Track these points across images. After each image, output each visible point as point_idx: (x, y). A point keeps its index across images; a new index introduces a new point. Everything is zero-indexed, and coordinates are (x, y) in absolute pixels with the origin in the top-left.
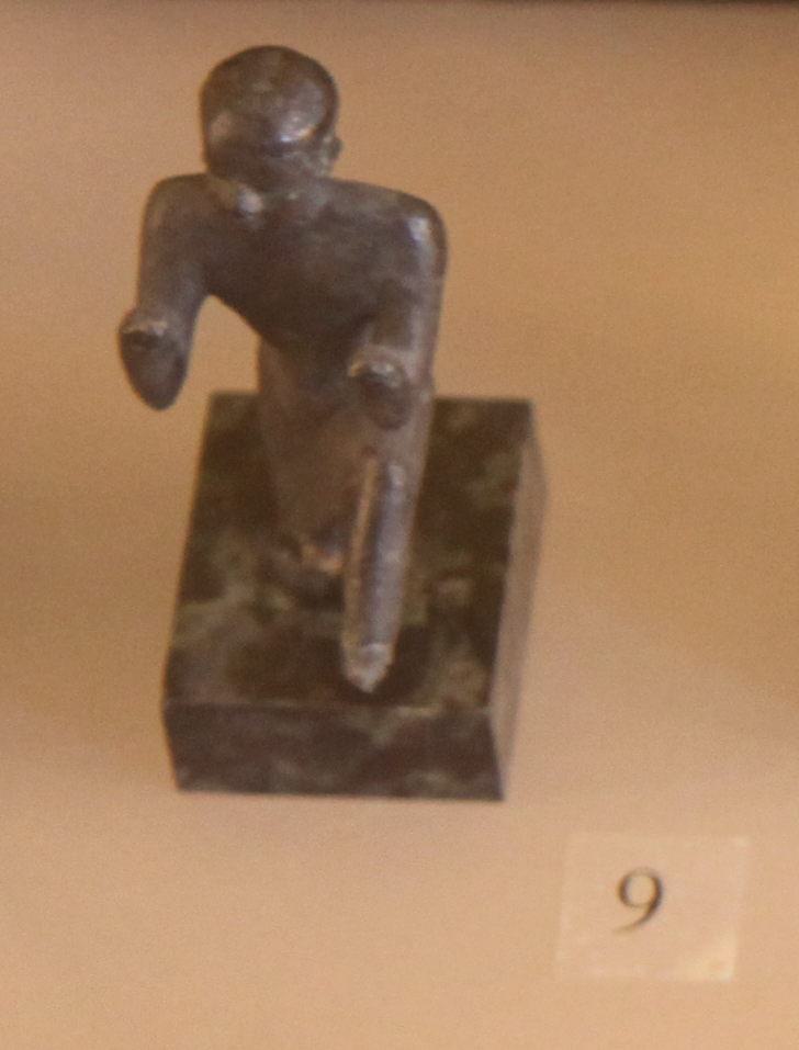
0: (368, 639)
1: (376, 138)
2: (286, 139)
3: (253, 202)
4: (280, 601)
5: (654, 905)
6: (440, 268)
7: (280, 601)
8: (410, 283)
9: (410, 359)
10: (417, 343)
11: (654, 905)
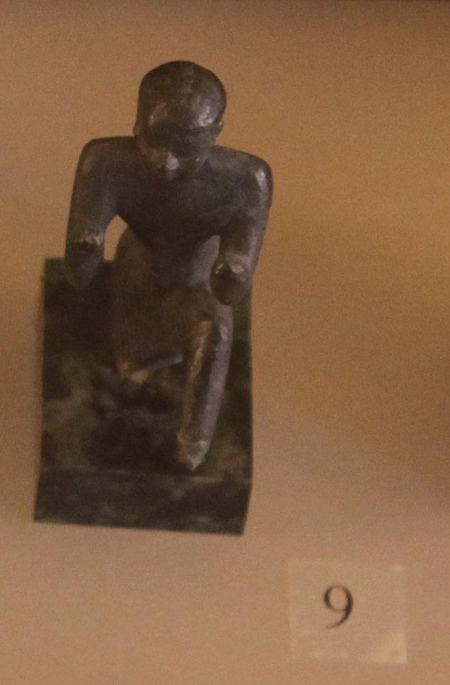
0: (196, 438)
1: (241, 125)
2: (202, 124)
3: (173, 163)
4: (108, 402)
5: (348, 609)
6: (269, 205)
7: (108, 402)
8: (252, 213)
9: (248, 260)
10: (252, 252)
11: (327, 598)
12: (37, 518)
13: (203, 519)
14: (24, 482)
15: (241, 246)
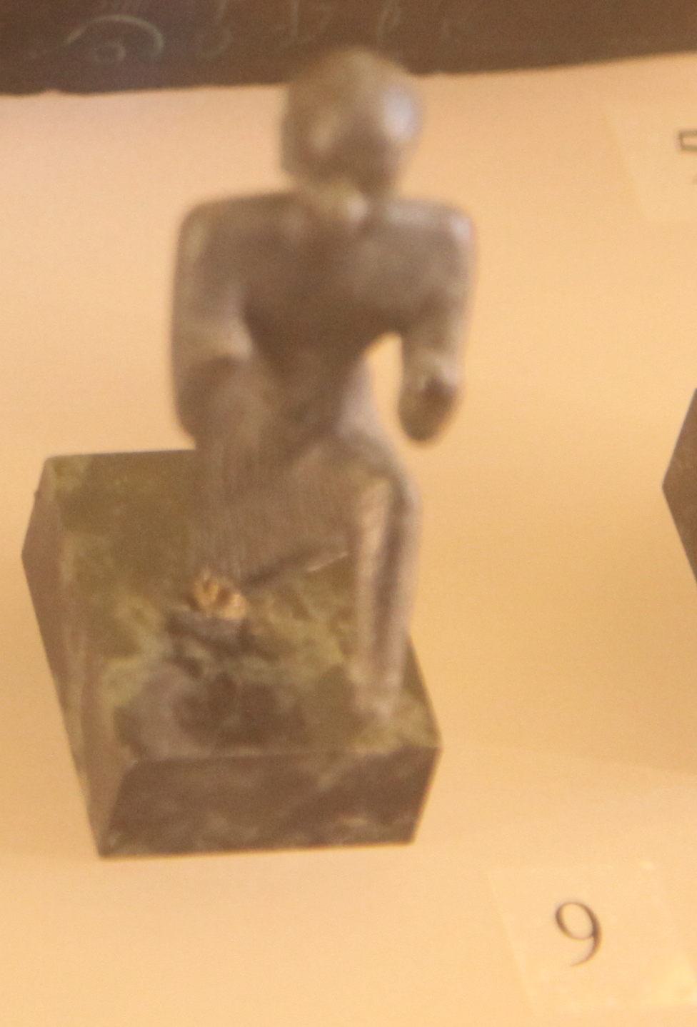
4: (198, 652)
5: (595, 933)
7: (198, 652)
12: (106, 851)
13: (358, 822)
14: (68, 803)
15: (440, 341)
